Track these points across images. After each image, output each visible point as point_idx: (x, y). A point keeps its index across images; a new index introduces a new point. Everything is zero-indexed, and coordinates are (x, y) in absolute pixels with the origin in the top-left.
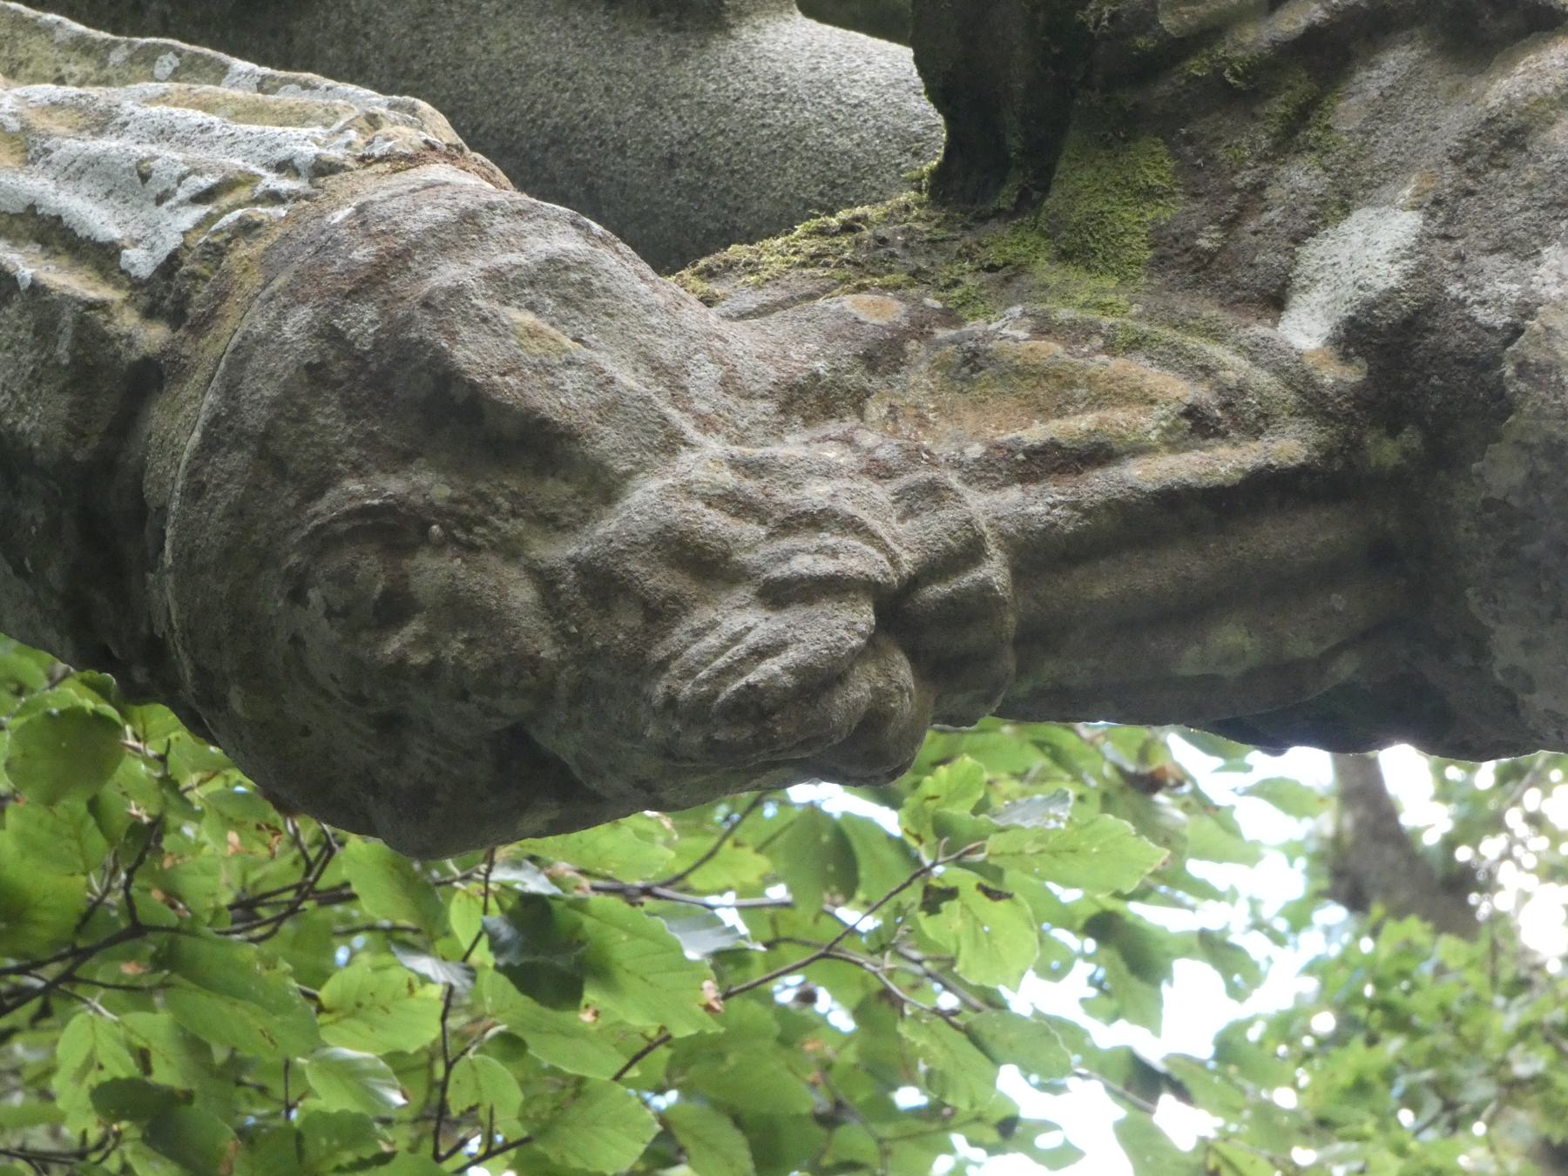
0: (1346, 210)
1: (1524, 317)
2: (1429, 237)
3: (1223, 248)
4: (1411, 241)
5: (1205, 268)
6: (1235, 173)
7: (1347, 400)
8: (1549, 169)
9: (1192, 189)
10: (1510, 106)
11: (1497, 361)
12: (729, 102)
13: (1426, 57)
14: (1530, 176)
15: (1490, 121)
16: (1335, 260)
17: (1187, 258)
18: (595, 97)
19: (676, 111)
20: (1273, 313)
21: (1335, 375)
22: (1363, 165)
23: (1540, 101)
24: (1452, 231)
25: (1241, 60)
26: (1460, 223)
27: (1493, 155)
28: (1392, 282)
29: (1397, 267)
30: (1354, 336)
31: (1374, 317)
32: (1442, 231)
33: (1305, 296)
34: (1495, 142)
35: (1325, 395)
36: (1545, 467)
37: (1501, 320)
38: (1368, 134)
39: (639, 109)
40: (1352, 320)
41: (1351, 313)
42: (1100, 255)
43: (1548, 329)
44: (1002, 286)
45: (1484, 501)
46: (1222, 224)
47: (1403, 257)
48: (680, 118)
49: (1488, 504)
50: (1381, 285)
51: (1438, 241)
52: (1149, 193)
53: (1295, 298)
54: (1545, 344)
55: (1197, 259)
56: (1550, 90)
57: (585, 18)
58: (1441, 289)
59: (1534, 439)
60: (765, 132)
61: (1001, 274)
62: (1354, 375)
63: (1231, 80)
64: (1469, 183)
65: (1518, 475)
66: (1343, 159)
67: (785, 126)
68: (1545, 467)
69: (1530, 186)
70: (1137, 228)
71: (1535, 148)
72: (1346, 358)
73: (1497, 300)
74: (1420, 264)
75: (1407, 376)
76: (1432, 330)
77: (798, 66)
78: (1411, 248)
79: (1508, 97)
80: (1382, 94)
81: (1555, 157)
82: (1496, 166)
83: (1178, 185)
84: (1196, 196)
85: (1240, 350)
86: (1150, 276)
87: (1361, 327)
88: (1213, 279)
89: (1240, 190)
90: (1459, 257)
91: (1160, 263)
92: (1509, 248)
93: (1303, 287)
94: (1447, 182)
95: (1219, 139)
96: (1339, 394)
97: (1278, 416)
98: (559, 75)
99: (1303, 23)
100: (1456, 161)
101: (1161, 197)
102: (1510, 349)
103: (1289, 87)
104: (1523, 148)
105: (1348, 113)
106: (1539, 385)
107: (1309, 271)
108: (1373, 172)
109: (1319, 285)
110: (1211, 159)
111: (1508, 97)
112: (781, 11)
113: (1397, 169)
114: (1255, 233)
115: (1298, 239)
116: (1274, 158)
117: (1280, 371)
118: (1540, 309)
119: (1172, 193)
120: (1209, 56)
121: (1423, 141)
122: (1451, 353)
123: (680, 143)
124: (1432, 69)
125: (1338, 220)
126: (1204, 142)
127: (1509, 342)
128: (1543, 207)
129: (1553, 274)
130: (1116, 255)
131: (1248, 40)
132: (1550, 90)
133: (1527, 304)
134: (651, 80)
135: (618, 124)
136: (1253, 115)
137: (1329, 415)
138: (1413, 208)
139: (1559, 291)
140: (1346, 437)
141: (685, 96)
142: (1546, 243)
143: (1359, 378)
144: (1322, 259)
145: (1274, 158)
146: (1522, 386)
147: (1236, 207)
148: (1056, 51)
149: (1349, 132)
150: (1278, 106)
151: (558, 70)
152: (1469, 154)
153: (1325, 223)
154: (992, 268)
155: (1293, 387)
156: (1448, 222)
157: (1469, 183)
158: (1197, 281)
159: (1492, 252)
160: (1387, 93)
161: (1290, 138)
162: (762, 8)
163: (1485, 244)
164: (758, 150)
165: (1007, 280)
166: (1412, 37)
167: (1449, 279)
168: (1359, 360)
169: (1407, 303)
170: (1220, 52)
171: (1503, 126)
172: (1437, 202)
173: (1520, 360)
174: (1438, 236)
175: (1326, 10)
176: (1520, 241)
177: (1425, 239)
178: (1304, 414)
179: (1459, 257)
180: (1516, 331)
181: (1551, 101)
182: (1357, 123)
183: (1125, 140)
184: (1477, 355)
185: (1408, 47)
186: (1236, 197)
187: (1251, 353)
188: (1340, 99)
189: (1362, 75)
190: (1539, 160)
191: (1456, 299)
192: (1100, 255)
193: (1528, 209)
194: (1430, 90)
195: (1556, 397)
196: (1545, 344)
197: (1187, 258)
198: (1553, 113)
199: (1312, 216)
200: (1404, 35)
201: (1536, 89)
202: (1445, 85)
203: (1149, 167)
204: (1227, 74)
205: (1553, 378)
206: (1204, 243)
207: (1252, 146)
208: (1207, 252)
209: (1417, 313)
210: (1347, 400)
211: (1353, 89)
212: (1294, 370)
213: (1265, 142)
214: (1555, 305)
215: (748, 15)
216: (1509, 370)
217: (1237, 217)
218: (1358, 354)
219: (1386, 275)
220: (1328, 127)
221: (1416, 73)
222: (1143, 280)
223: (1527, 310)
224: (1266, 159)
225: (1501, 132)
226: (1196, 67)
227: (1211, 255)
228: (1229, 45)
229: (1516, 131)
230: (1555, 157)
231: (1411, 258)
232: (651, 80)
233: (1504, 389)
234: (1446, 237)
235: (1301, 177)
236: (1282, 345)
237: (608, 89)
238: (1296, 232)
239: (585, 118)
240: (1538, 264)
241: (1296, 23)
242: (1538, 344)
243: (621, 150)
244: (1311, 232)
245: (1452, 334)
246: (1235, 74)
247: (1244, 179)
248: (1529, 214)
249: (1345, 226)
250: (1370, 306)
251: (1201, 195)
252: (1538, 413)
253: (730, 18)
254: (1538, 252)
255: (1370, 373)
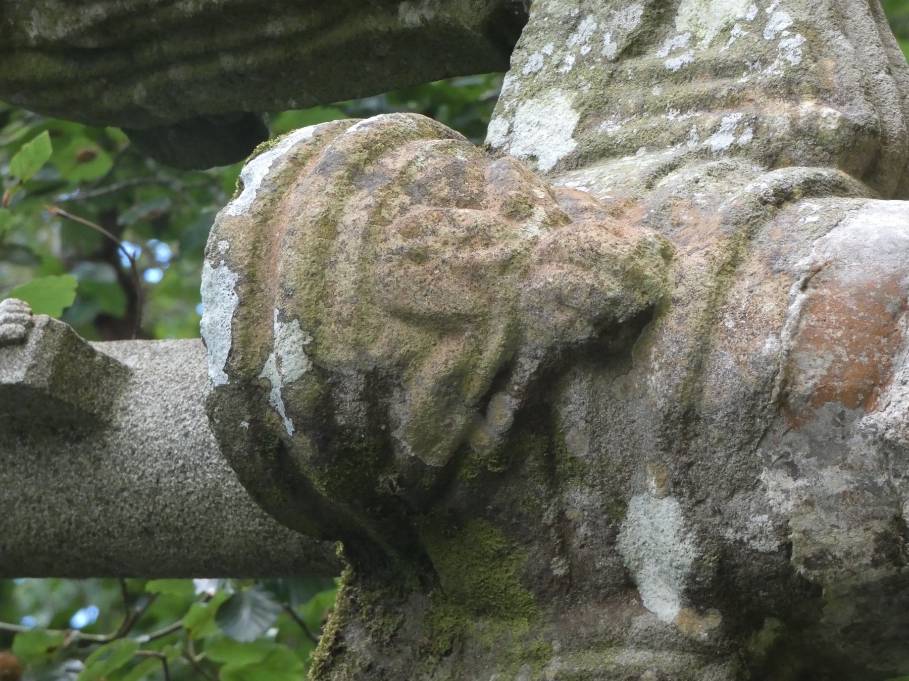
0: (623, 504)
1: (786, 535)
2: (690, 510)
3: (571, 566)
4: (681, 521)
5: (571, 586)
6: (541, 517)
7: (724, 640)
8: (723, 425)
9: (524, 539)
10: (672, 401)
11: (792, 569)
12: (154, 485)
13: (592, 380)
14: (716, 433)
15: (667, 417)
16: (642, 540)
17: (556, 587)
18: (65, 509)
19: (125, 501)
20: (632, 593)
21: (704, 628)
22: (611, 470)
23: (685, 387)
24: (699, 495)
25: (491, 455)
26: (699, 488)
27: (684, 434)
28: (694, 555)
29: (687, 542)
30: (696, 597)
31: (699, 583)
32: (694, 500)
33: (643, 571)
34: (680, 426)
35: (709, 647)
36: (862, 600)
37: (774, 545)
38: (598, 450)
39: (100, 508)
40: (687, 591)
41: (684, 587)
42: (503, 608)
43: (804, 532)
44: (461, 659)
45: (842, 631)
46: (559, 554)
47: (686, 533)
48: (131, 505)
49: (846, 631)
50: (688, 561)
51: (696, 508)
52: (500, 555)
53: (638, 576)
54: (809, 542)
55: (562, 583)
56: (685, 374)
57: (15, 454)
58: (722, 538)
59: (846, 592)
60: (193, 497)
61: (455, 654)
62: (714, 620)
63: (496, 470)
64: (684, 459)
65: (851, 610)
66: (596, 475)
67: (202, 490)
68: (862, 600)
69: (720, 440)
70: (511, 581)
71: (705, 413)
72: (702, 613)
73: (761, 532)
74: (698, 532)
75: (743, 597)
76: (737, 566)
77: (175, 436)
78: (686, 525)
79: (665, 396)
80: (587, 422)
81: (721, 414)
82: (691, 438)
83: (513, 542)
84: (529, 543)
85: (639, 646)
86: (543, 609)
87: (697, 592)
88: (580, 589)
89: (552, 525)
90: (717, 512)
91: (542, 597)
92: (740, 487)
93: (637, 567)
94: (672, 467)
95: (515, 501)
96: (717, 640)
97: (694, 676)
98: (31, 503)
99: (510, 414)
100: (667, 450)
101: (509, 554)
102: (792, 559)
103: (531, 449)
104: (698, 418)
105: (576, 441)
106: (823, 566)
107: (633, 555)
108: (619, 470)
109: (646, 560)
110: (520, 515)
111: (665, 396)
112: (126, 380)
113: (631, 462)
114: (582, 546)
115: (612, 540)
116: (555, 493)
117: (672, 647)
118: (790, 523)
119: (513, 548)
120: (471, 463)
121: (632, 434)
122: (759, 577)
123: (144, 521)
124: (601, 383)
125: (623, 514)
126: (507, 508)
127: (789, 556)
128: (739, 450)
129: (779, 493)
130: (512, 604)
131: (486, 442)
132: (685, 374)
133: (781, 527)
134: (93, 486)
135: (95, 521)
136: (523, 476)
137: (722, 655)
138: (666, 496)
139: (791, 503)
140: (741, 659)
141: (123, 490)
142: (759, 471)
143: (719, 620)
144: (634, 543)
145: (555, 493)
146: (816, 572)
147: (558, 538)
148: (378, 509)
149: (587, 456)
150: (532, 463)
151: (27, 499)
152: (671, 442)
153: (618, 520)
154: (448, 653)
155: (687, 651)
156: (692, 494)
157: (684, 459)
158: (573, 597)
159: (732, 495)
160: (589, 419)
161: (556, 470)
162: (115, 391)
163: (724, 493)
164: (198, 510)
165: (462, 652)
166: (575, 374)
167: (722, 531)
168: (711, 611)
169: (711, 562)
170: (475, 457)
171: (677, 415)
172: (676, 484)
173: (803, 560)
174: (694, 505)
175: (516, 397)
176: (743, 480)
177: (688, 513)
178: (707, 663)
179: (717, 512)
180: (787, 547)
181: (691, 380)
182: (587, 448)
183: (460, 529)
184: (776, 571)
185: (577, 380)
186: (553, 530)
187: (647, 644)
188: (563, 434)
189: (564, 411)
190: (713, 420)
191: (736, 541)
192: (503, 608)
193: (731, 455)
194: (611, 398)
195: (840, 568)
196: (809, 542)
197: (556, 587)
198: (697, 385)
199: (608, 522)
200: (569, 376)
201: (677, 380)
202: (616, 388)
203: (487, 539)
204: (490, 469)
205: (830, 558)
206: (559, 572)
207: (537, 494)
208: (565, 576)
209: (720, 562)
210: (724, 640)
211: (567, 424)
212: (680, 641)
213: (542, 487)
214: (797, 515)
215: (111, 404)
216: (801, 569)
217: (563, 543)
218: (707, 607)
219: (686, 552)
220: (572, 459)
221: (594, 395)
222: (541, 613)
223: (783, 530)
224: (551, 497)
225: (678, 418)
226: (467, 473)
227: (568, 576)
228: (477, 450)
229: (687, 413)
230: (721, 414)
231: (689, 531)
232: (93, 486)
233: (808, 581)
234: (699, 502)
235: (580, 498)
236: (659, 627)
237: (70, 501)
238: (607, 538)
239: (70, 524)
240: (764, 490)
241: (506, 415)
242: (806, 544)
243: (109, 535)
244: (615, 532)
245: (751, 564)
246: (493, 465)
247: (549, 517)
248: (734, 458)
249: (630, 515)
250: (691, 578)
251: (532, 540)
252: (837, 580)
253: (105, 417)
254: (759, 480)
255: (722, 613)
